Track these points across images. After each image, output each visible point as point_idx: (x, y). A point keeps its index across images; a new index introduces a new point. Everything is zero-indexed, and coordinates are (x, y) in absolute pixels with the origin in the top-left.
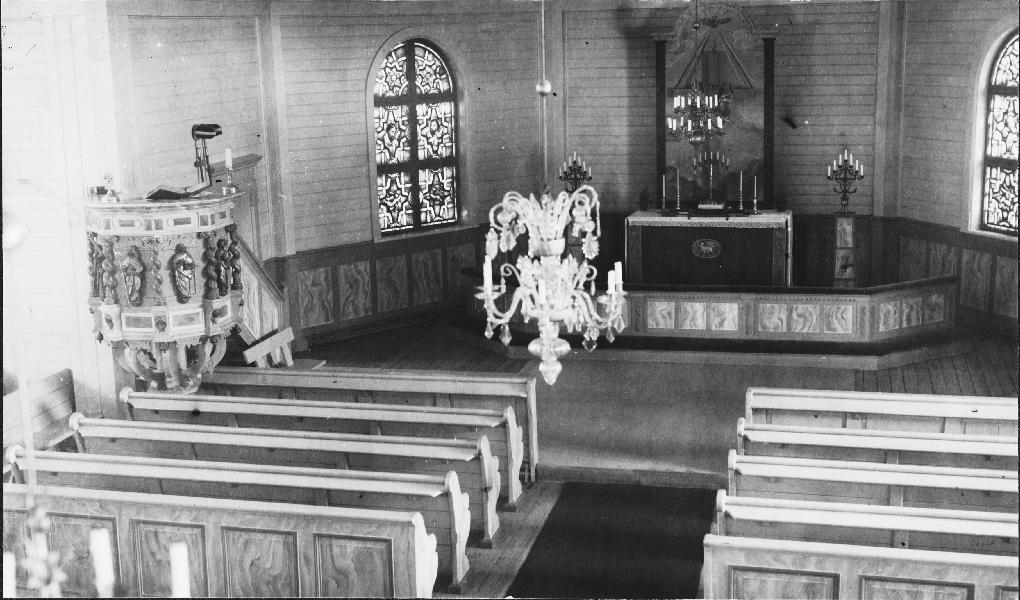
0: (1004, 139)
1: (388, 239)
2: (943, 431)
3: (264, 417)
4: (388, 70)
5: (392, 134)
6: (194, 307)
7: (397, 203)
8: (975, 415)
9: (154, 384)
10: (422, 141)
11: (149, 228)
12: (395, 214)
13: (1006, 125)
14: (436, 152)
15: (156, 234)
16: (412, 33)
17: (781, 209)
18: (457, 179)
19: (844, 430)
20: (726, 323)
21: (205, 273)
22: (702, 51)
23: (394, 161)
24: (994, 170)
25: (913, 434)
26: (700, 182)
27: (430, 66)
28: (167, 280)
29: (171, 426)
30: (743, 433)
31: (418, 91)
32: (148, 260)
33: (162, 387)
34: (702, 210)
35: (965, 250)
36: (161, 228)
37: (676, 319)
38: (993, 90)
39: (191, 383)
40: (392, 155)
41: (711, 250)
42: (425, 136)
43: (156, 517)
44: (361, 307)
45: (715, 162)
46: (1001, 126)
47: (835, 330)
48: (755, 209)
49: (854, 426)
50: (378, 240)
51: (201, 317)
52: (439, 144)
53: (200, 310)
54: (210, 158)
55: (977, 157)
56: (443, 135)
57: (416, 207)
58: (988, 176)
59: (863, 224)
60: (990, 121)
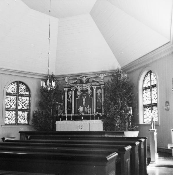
23: (11, 108)
52: (24, 106)
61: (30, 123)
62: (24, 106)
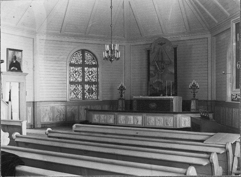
4: (76, 57)
5: (76, 74)
7: (77, 92)
8: (137, 134)
10: (86, 77)
27: (90, 58)
31: (86, 64)
47: (168, 125)
56: (93, 76)
57: (84, 94)
61: (99, 98)
62: (91, 78)
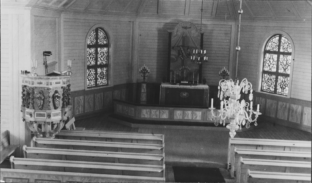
0: (269, 66)
1: (90, 89)
2: (284, 150)
3: (90, 147)
4: (91, 37)
6: (59, 111)
8: (100, 136)
9: (41, 135)
11: (47, 85)
12: (90, 81)
13: (270, 62)
14: (102, 63)
15: (50, 87)
16: (97, 26)
17: (204, 84)
18: (107, 71)
19: (284, 151)
20: (198, 117)
21: (63, 99)
22: (182, 36)
24: (266, 75)
25: (304, 152)
26: (180, 74)
27: (102, 36)
28: (52, 102)
29: (49, 149)
30: (236, 151)
32: (46, 95)
33: (44, 136)
34: (182, 83)
35: (257, 97)
36: (52, 85)
37: (183, 116)
38: (266, 52)
39: (54, 135)
40: (91, 63)
41: (186, 95)
42: (100, 58)
43: (75, 180)
44: (80, 111)
45: (186, 69)
46: (268, 62)
48: (198, 83)
49: (259, 149)
50: (87, 89)
51: (61, 114)
52: (103, 60)
53: (60, 112)
54: (47, 62)
55: (261, 70)
56: (104, 57)
57: (96, 79)
58: (264, 76)
59: (148, 85)
60: (265, 61)
